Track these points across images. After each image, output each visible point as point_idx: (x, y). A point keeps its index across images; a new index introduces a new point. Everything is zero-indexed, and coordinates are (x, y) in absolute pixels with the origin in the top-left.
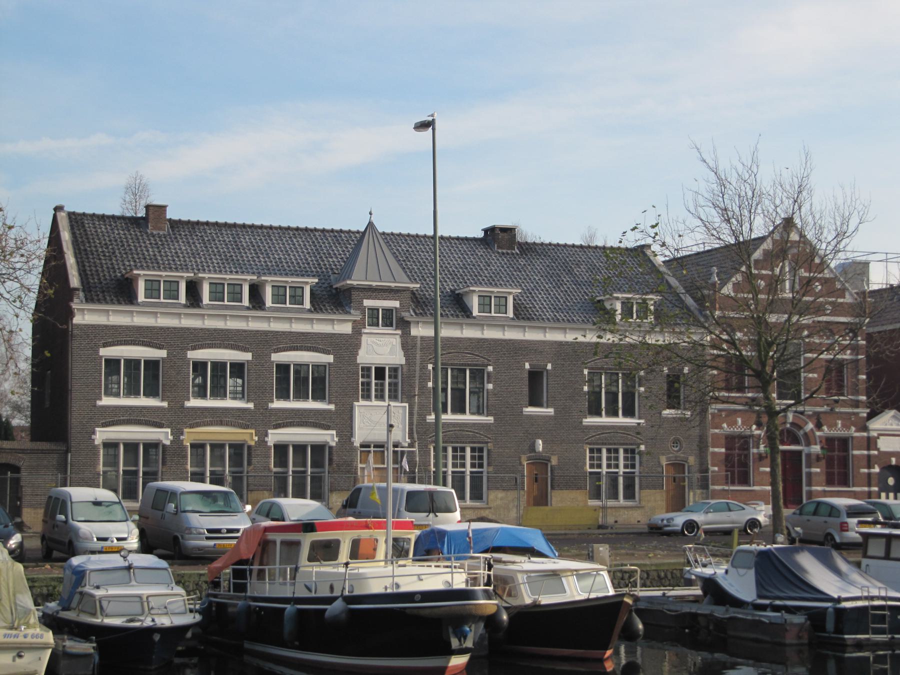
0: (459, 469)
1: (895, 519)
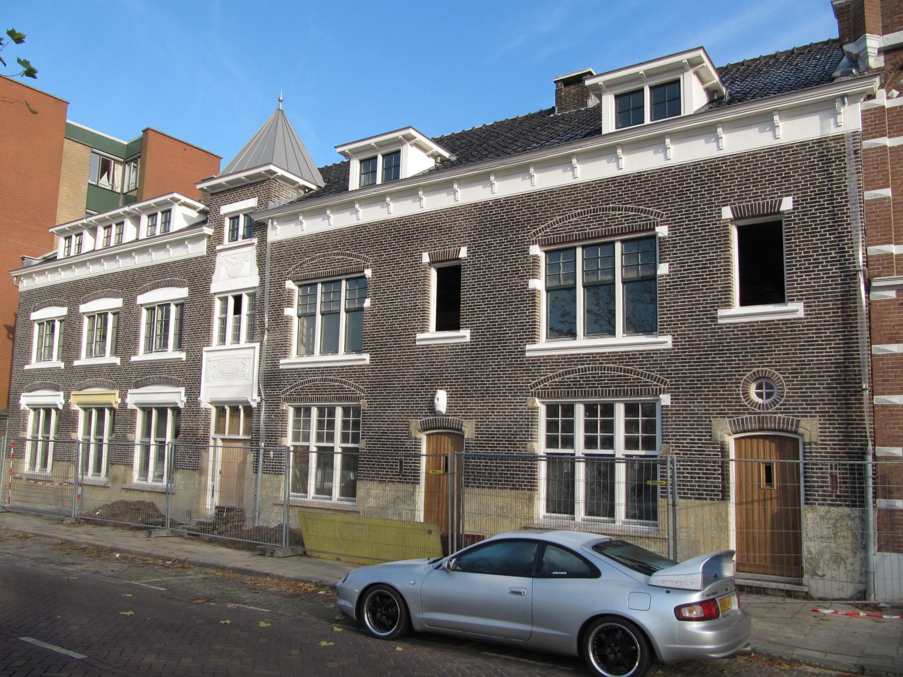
0: (350, 445)
1: (483, 538)
